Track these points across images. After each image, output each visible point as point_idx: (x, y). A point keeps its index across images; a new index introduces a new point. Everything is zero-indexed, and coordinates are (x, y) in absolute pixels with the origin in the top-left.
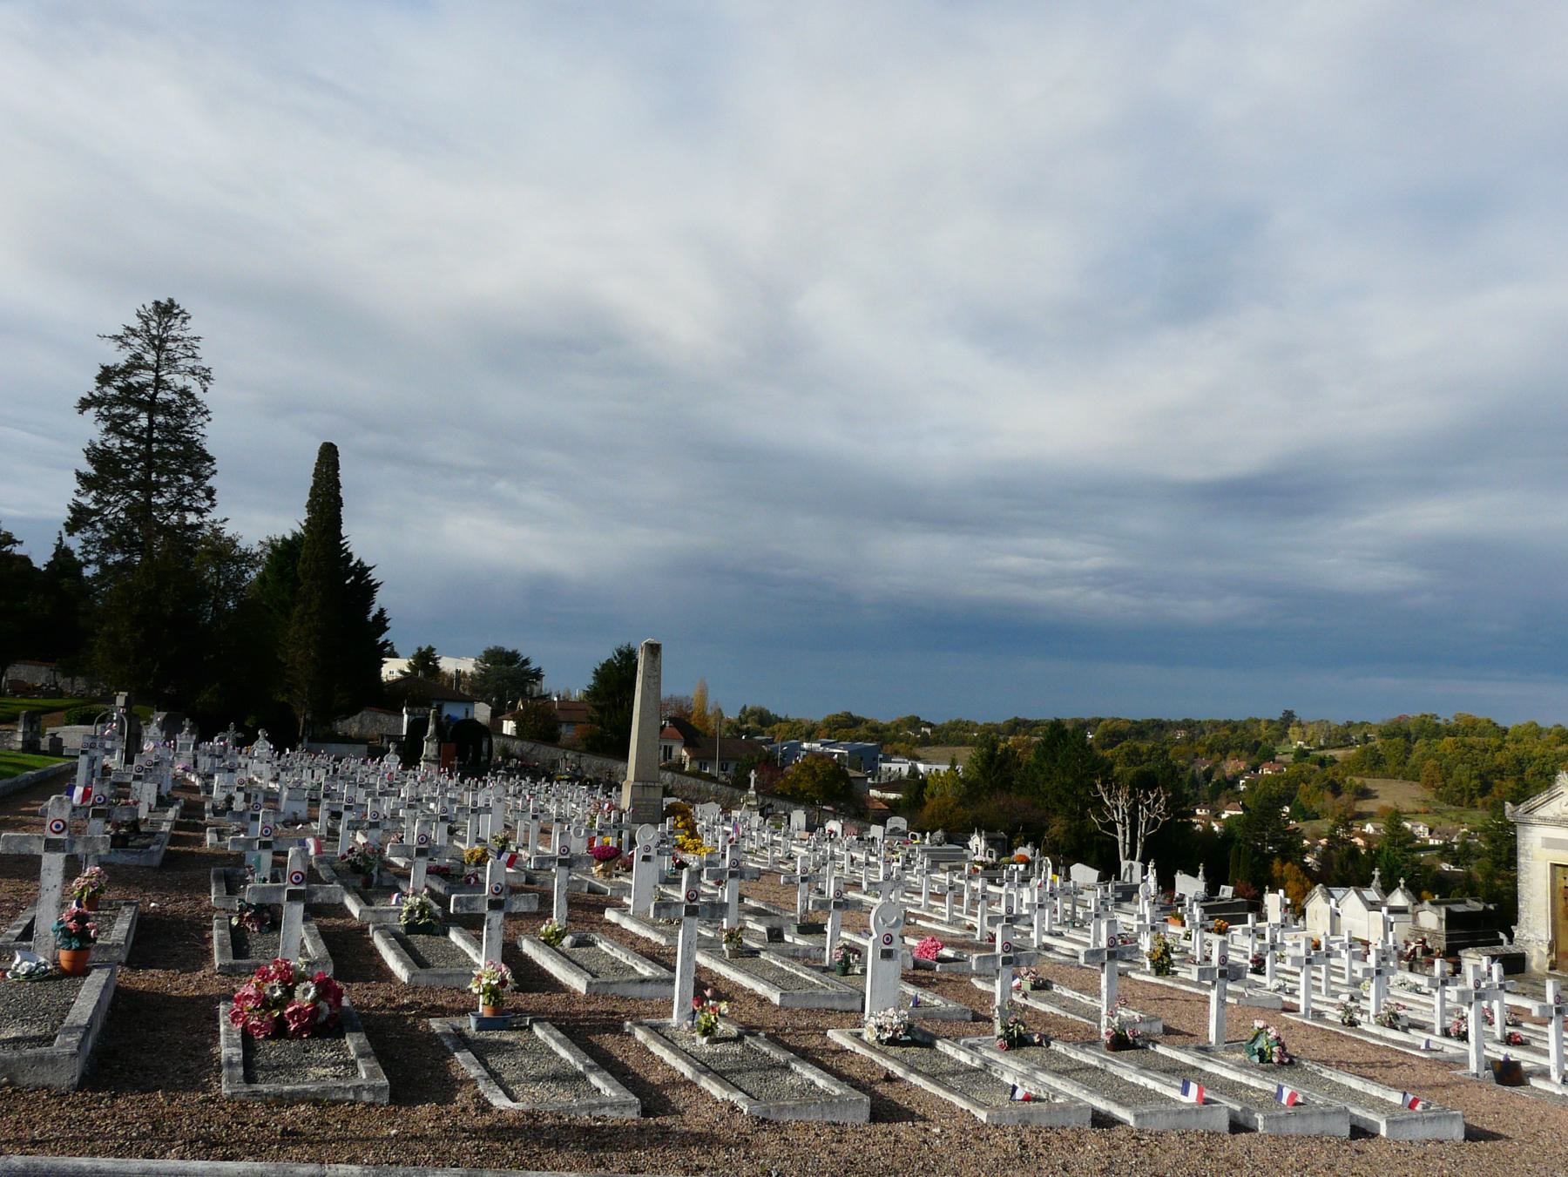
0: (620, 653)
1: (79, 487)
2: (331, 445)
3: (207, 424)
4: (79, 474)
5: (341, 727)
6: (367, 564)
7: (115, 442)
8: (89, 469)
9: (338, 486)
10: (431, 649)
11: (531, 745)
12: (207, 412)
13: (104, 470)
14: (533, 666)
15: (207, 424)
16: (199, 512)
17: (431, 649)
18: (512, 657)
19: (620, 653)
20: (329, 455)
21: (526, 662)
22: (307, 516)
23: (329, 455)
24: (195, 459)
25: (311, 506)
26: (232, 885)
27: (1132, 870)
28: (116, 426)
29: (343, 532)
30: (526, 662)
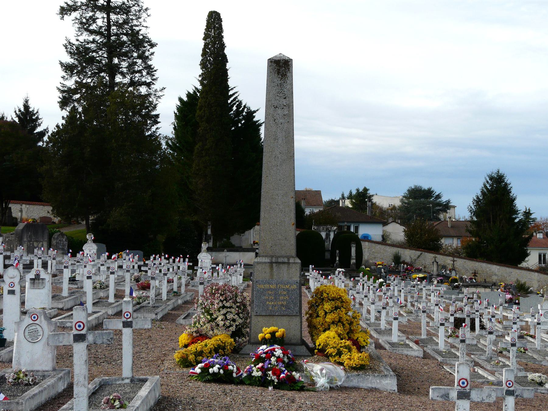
0: (491, 178)
1: (64, 74)
2: (215, 12)
3: (148, 19)
4: (61, 64)
5: (235, 240)
6: (253, 109)
7: (85, 36)
8: (68, 60)
9: (223, 46)
10: (366, 190)
11: (418, 253)
12: (146, 9)
13: (80, 58)
14: (444, 199)
15: (148, 19)
16: (148, 85)
17: (366, 190)
18: (429, 193)
19: (491, 178)
20: (214, 21)
21: (438, 196)
22: (201, 72)
23: (214, 21)
24: (140, 43)
25: (203, 65)
26: (335, 361)
27: (448, 220)
28: (85, 25)
29: (231, 83)
30: (438, 196)
